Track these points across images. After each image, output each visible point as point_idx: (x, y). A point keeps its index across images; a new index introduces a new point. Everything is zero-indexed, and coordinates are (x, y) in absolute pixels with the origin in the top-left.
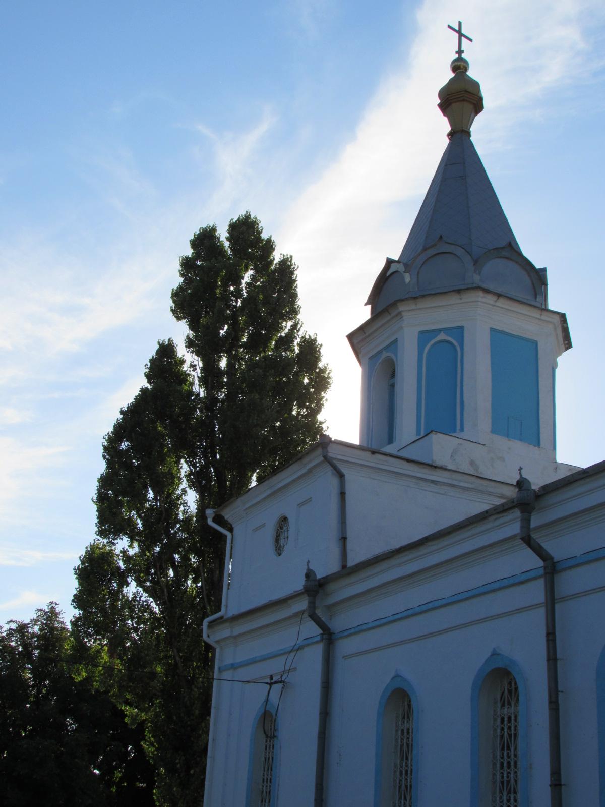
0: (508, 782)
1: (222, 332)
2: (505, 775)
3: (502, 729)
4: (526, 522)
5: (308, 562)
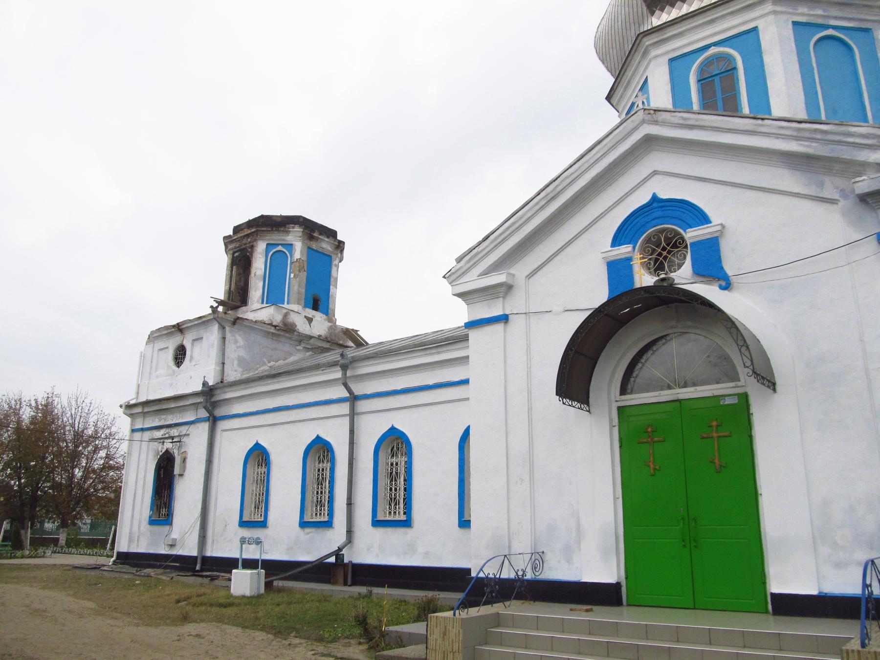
0: (321, 501)
1: (32, 463)
2: (319, 498)
3: (318, 475)
4: (345, 374)
5: (204, 377)
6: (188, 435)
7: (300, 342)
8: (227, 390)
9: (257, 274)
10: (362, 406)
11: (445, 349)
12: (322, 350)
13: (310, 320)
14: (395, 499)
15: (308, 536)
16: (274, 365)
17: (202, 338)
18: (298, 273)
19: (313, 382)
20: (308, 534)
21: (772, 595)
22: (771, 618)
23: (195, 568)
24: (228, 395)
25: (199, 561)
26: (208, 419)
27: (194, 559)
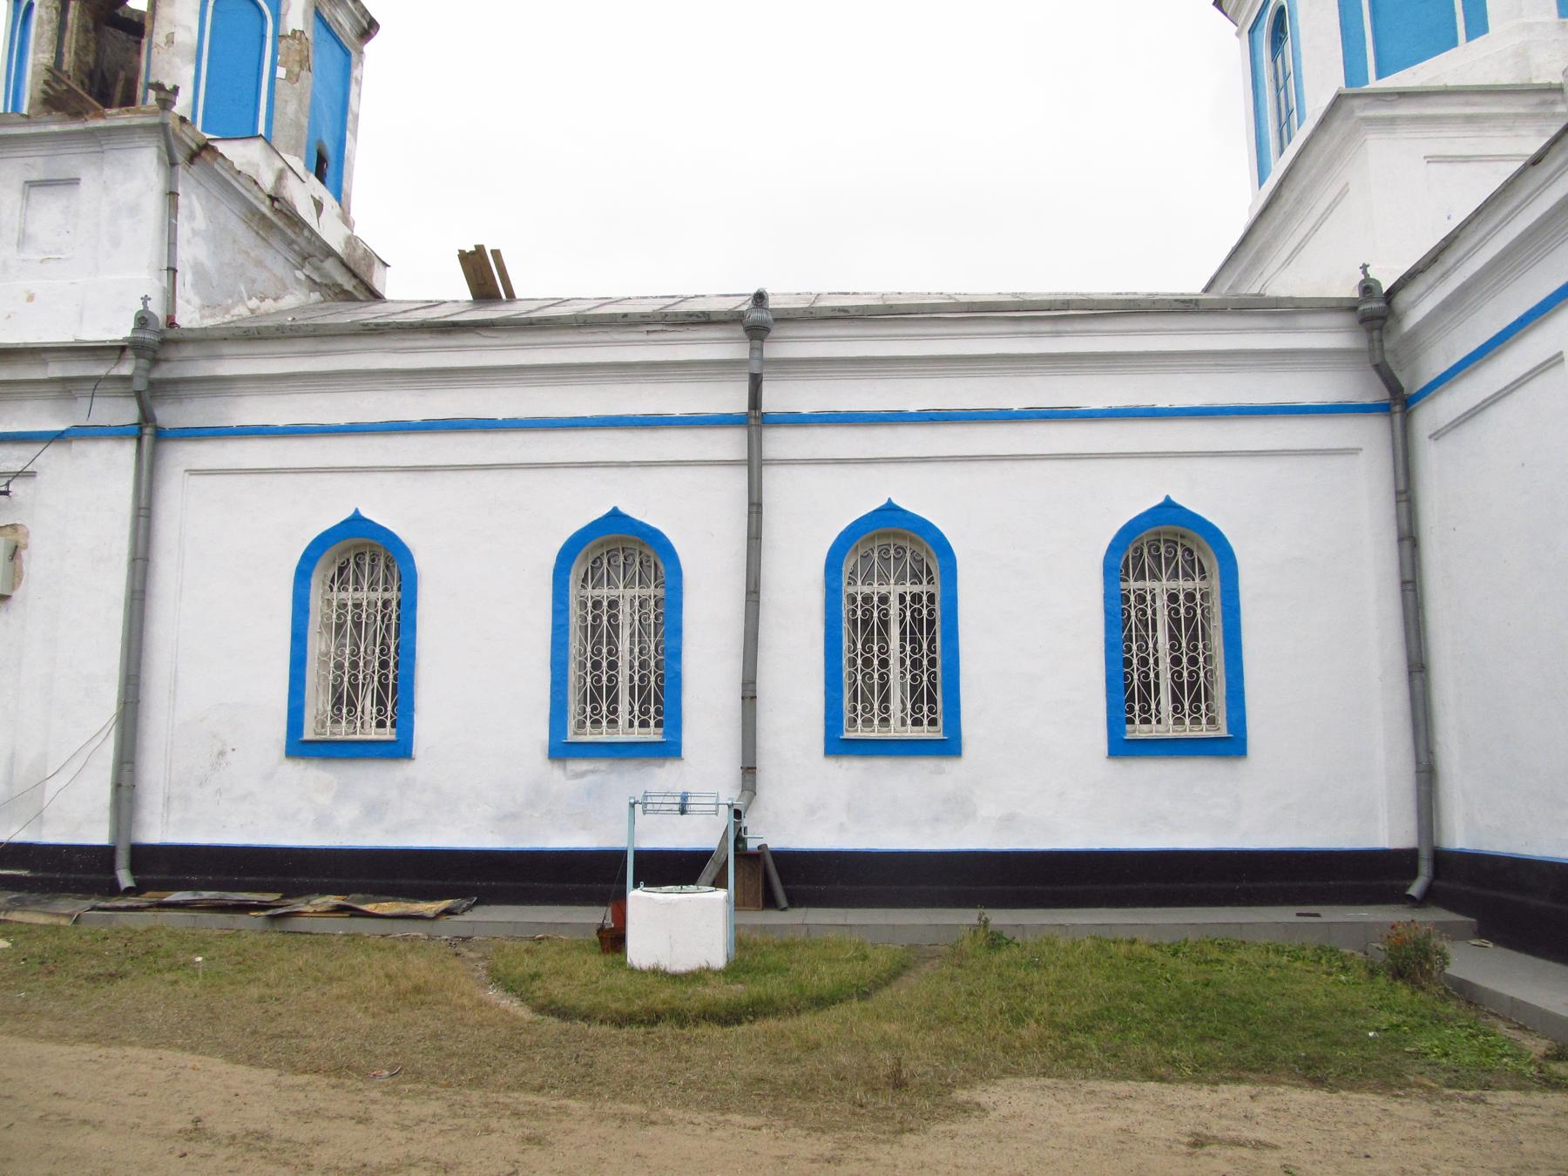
5: (1364, 267)
6: (32, 474)
7: (305, 257)
8: (226, 349)
9: (178, 38)
10: (778, 442)
11: (1078, 326)
12: (336, 294)
13: (319, 206)
14: (1192, 685)
15: (578, 782)
16: (258, 308)
17: (74, 182)
18: (296, 69)
19: (1482, 342)
20: (582, 775)
21: (726, 887)
22: (733, 924)
23: (1407, 887)
24: (227, 368)
25: (122, 860)
26: (136, 433)
27: (103, 856)
